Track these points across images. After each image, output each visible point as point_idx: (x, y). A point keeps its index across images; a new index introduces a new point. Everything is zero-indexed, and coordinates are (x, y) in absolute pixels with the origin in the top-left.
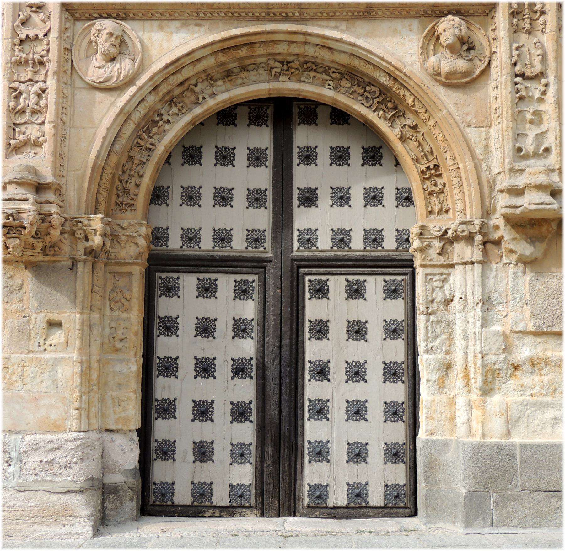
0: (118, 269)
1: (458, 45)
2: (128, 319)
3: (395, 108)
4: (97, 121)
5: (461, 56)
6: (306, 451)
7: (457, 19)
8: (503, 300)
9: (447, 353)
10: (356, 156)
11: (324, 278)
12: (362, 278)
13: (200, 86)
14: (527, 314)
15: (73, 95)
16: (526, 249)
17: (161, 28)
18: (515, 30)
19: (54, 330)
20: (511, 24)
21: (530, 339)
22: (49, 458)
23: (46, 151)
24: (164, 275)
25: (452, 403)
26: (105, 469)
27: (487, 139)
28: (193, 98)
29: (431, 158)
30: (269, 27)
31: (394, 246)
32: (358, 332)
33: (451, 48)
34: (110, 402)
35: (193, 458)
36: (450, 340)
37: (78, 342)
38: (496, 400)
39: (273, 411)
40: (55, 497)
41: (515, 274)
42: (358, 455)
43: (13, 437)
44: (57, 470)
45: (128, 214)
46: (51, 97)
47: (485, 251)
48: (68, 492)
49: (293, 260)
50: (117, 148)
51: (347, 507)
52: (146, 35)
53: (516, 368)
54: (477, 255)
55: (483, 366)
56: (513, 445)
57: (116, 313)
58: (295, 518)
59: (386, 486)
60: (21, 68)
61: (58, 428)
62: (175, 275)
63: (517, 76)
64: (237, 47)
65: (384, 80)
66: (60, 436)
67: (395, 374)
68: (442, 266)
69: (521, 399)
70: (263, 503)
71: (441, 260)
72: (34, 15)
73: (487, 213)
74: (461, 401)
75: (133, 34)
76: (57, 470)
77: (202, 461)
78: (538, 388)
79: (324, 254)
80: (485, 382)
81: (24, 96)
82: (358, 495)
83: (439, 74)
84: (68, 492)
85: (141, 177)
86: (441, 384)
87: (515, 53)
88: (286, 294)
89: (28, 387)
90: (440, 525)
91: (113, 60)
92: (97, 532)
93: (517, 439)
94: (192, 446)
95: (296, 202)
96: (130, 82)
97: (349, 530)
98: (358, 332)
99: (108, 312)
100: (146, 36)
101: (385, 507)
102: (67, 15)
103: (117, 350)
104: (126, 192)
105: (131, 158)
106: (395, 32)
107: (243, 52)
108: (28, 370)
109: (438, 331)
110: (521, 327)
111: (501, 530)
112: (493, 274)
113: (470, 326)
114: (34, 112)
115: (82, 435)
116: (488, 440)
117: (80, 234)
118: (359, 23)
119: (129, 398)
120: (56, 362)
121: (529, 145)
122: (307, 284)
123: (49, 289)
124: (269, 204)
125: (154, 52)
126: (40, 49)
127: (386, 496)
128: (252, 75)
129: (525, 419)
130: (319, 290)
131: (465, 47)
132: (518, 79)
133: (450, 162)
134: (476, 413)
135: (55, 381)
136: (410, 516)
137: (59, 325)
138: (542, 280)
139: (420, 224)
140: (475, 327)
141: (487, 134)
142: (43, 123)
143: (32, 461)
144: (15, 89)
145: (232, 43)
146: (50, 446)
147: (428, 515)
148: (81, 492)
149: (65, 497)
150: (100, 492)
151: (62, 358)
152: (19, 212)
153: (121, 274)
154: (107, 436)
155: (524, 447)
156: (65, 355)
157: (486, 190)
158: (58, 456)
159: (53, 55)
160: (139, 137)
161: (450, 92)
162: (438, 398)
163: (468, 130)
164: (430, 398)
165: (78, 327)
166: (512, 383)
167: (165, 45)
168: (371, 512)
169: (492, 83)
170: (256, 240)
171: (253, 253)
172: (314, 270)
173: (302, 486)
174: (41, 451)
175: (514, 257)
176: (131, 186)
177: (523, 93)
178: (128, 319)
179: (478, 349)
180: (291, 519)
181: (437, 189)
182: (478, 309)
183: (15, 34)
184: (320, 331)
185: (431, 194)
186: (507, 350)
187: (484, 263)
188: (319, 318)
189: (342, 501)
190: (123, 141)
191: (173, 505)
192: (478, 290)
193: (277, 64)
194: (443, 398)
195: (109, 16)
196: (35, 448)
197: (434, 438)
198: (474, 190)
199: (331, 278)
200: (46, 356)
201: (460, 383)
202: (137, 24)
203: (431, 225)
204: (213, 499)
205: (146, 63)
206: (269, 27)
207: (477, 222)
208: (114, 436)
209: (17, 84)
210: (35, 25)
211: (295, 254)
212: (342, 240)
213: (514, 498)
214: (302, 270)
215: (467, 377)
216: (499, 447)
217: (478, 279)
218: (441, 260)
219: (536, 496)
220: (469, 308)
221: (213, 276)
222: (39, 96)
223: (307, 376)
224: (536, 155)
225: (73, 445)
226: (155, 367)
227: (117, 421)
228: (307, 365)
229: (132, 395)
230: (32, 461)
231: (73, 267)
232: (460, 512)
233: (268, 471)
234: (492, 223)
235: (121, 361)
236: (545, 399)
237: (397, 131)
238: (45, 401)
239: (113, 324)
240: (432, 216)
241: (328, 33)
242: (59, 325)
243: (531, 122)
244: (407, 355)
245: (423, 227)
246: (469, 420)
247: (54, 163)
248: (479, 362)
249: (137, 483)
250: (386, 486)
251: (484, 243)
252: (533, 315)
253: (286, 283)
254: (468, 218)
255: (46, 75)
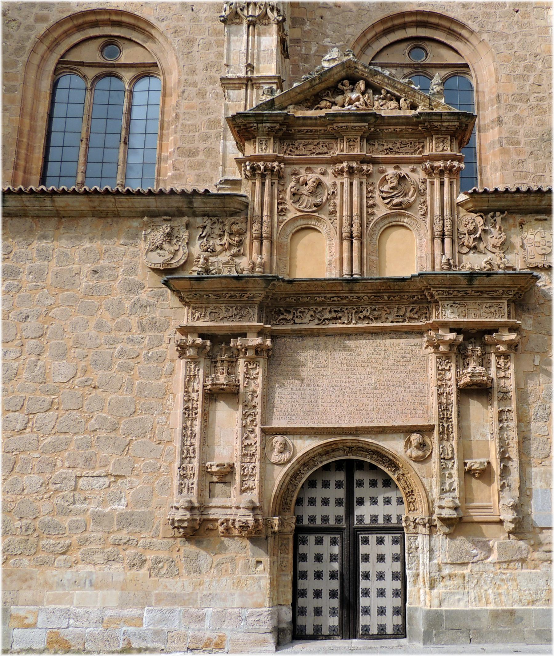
0: (283, 536)
1: (419, 446)
2: (288, 557)
3: (395, 466)
4: (275, 478)
5: (420, 450)
6: (360, 611)
7: (418, 435)
8: (438, 549)
9: (417, 569)
10: (380, 484)
11: (367, 536)
12: (383, 535)
13: (316, 458)
14: (447, 556)
15: (266, 466)
16: (447, 530)
17: (301, 438)
18: (441, 440)
19: (258, 564)
20: (440, 437)
21: (449, 566)
22: (258, 619)
23: (256, 492)
24: (301, 536)
25: (419, 591)
26: (279, 621)
27: (431, 483)
28: (313, 463)
29: (410, 487)
30: (344, 438)
31: (396, 522)
32: (381, 559)
33: (416, 447)
34: (280, 593)
35: (314, 614)
36: (418, 563)
37: (269, 570)
38: (435, 591)
39: (346, 593)
40: (260, 635)
41: (442, 539)
42: (382, 612)
43: (243, 610)
44: (261, 624)
45: (287, 513)
46: (258, 470)
47: (431, 531)
48: (266, 633)
49: (355, 528)
50: (283, 487)
51: (377, 635)
52: (295, 441)
53: (443, 578)
54: (427, 532)
55: (430, 577)
56: (442, 611)
57: (283, 555)
58: (356, 640)
59: (394, 625)
60: (245, 457)
61: (261, 606)
62: (306, 536)
63: (442, 459)
64: (331, 445)
65: (391, 457)
66: (262, 609)
67: (397, 577)
68: (415, 533)
69: (445, 591)
70: (343, 633)
71: (414, 531)
72: (250, 435)
73: (431, 514)
74: (422, 591)
75: (289, 442)
76: (261, 624)
77: (318, 616)
78: (452, 586)
79: (367, 526)
80: (431, 584)
81: (246, 469)
82: (382, 629)
83: (412, 457)
84: (266, 633)
85: (292, 497)
86: (415, 583)
87: (441, 449)
88: (352, 542)
89: (249, 589)
90: (414, 643)
91: (281, 453)
92: (277, 650)
93: (444, 608)
94: (313, 609)
95: (355, 504)
96: (289, 461)
97: (377, 646)
98: (381, 559)
99: (279, 554)
100: (294, 442)
101: (393, 634)
102: (263, 434)
103: (283, 571)
104: (286, 503)
105: (288, 489)
106: (394, 439)
107: (334, 446)
108: (249, 582)
109: (413, 560)
110: (445, 561)
111: (437, 646)
112: (434, 539)
113: (425, 560)
114: (250, 476)
115: (271, 609)
116: (432, 608)
117: (269, 526)
118: (379, 435)
119: (289, 591)
120: (260, 578)
121: (447, 487)
122: (360, 538)
123: (257, 548)
124: (344, 504)
125: (298, 448)
126: (253, 449)
127: (393, 629)
128: (337, 453)
129: (447, 599)
130: (365, 541)
131: (422, 446)
132: (442, 461)
133: (417, 491)
134: (428, 597)
135: (259, 586)
136: (404, 638)
137: (261, 562)
138: (453, 541)
139: (406, 516)
140: (427, 561)
141: (431, 481)
142: (254, 480)
143: (251, 620)
144: (243, 466)
145: (329, 444)
146: (258, 614)
147: (410, 639)
148: (270, 633)
149: (264, 635)
150: (276, 633)
151: (262, 577)
152: (247, 521)
153: (285, 539)
154: (279, 607)
155: (446, 611)
156: (263, 575)
157: (431, 505)
158: (261, 618)
159: (258, 452)
160: (292, 480)
161: (416, 464)
162: (413, 589)
163: (423, 479)
164: (410, 589)
165: (269, 564)
166: (442, 584)
167: (302, 445)
168: (388, 637)
169: (433, 461)
170: (339, 520)
171: (338, 525)
172: (363, 532)
173: (359, 626)
174: (254, 616)
175: (442, 533)
176: (288, 501)
177: (444, 466)
178: (288, 557)
179: (428, 571)
180: (354, 641)
181: (412, 501)
182: (428, 554)
183: (243, 443)
184: (366, 559)
185: (410, 502)
186: (440, 570)
187: (430, 535)
188: (365, 553)
189: (376, 632)
190: (285, 484)
191: (306, 635)
192: (428, 546)
193: (347, 449)
194: (416, 589)
195: (280, 434)
196: (252, 615)
197: (412, 606)
198: (426, 505)
199: (370, 535)
200: (256, 576)
201: (422, 584)
202: (291, 437)
203: (410, 516)
204: (322, 632)
205: (295, 453)
206: (344, 438)
207: (427, 519)
208: (282, 607)
209: (243, 464)
210: (250, 439)
211: (355, 526)
212: (374, 520)
213: (442, 632)
214: (358, 532)
215: (424, 581)
216: (436, 612)
217: (428, 542)
218: (414, 531)
219: (451, 632)
220: (425, 552)
221: (321, 535)
222: (253, 469)
223: (361, 578)
224: (450, 491)
225: (267, 613)
226: (298, 575)
227: (283, 601)
228: (361, 573)
229: (289, 590)
230: (251, 620)
231: (267, 538)
232: (421, 638)
233: (345, 619)
234: (433, 518)
235: (285, 575)
236: (455, 591)
237: (396, 476)
238: (256, 595)
239: (282, 560)
240: (411, 512)
241: (367, 440)
242: (261, 562)
243: (448, 477)
244: (401, 569)
245: (407, 517)
246: (425, 599)
247: (259, 499)
248: (428, 576)
249: (291, 627)
250: (394, 625)
251: (430, 527)
252: (450, 556)
253: (352, 538)
254: (424, 517)
255: (255, 460)
